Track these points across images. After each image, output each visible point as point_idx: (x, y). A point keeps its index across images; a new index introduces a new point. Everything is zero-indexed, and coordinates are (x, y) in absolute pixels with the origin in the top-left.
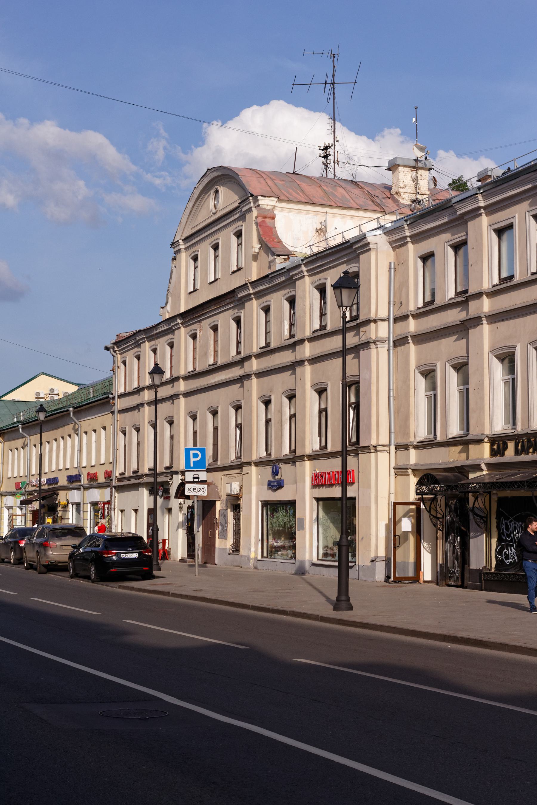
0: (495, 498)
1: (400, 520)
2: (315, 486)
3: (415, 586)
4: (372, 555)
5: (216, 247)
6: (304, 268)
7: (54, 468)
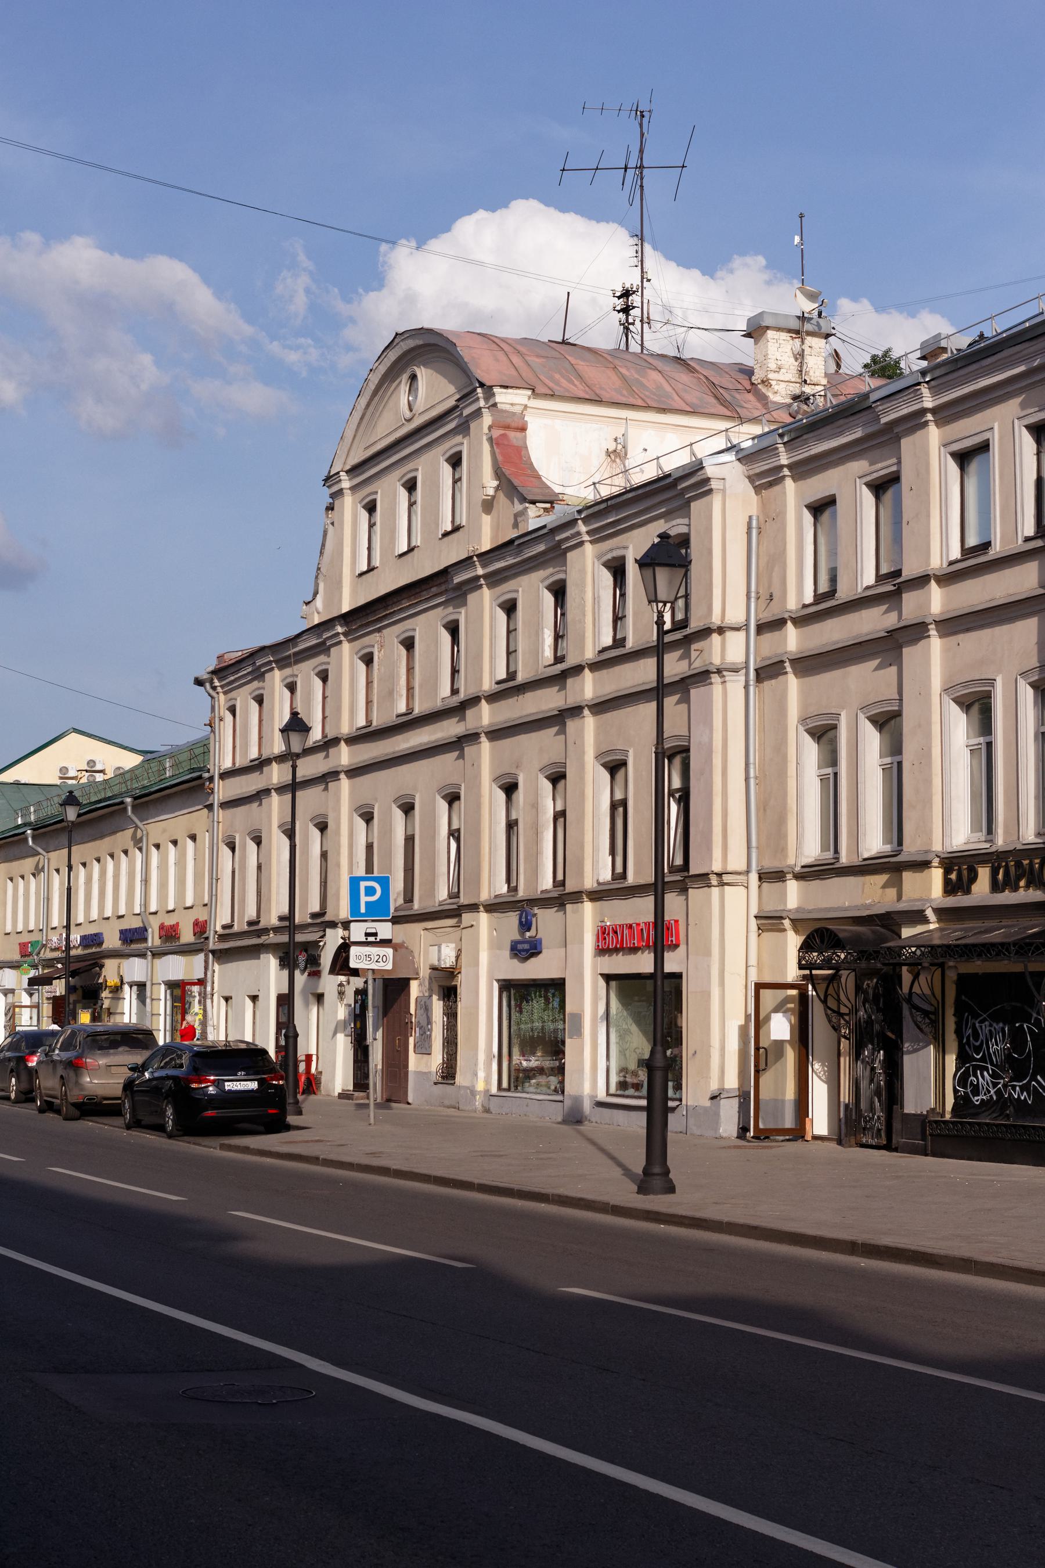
0: (952, 975)
1: (768, 1018)
2: (602, 951)
3: (799, 1145)
4: (714, 1086)
5: (411, 486)
6: (582, 528)
7: (94, 915)
